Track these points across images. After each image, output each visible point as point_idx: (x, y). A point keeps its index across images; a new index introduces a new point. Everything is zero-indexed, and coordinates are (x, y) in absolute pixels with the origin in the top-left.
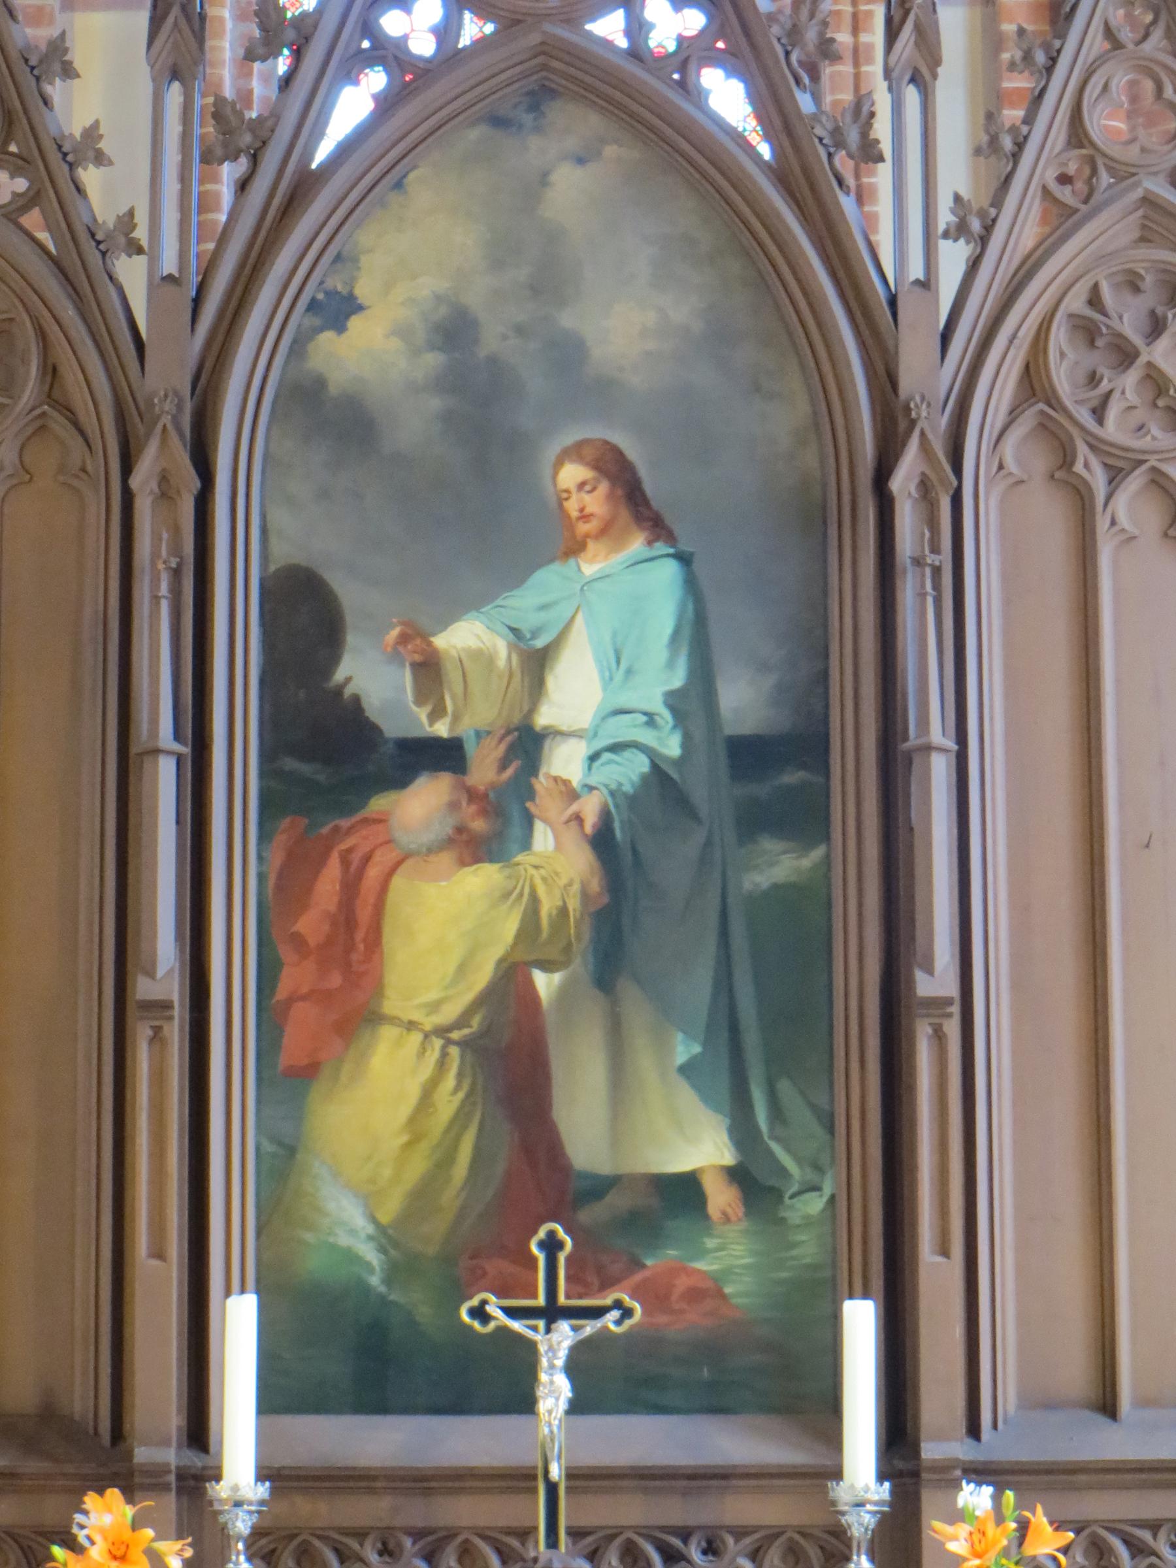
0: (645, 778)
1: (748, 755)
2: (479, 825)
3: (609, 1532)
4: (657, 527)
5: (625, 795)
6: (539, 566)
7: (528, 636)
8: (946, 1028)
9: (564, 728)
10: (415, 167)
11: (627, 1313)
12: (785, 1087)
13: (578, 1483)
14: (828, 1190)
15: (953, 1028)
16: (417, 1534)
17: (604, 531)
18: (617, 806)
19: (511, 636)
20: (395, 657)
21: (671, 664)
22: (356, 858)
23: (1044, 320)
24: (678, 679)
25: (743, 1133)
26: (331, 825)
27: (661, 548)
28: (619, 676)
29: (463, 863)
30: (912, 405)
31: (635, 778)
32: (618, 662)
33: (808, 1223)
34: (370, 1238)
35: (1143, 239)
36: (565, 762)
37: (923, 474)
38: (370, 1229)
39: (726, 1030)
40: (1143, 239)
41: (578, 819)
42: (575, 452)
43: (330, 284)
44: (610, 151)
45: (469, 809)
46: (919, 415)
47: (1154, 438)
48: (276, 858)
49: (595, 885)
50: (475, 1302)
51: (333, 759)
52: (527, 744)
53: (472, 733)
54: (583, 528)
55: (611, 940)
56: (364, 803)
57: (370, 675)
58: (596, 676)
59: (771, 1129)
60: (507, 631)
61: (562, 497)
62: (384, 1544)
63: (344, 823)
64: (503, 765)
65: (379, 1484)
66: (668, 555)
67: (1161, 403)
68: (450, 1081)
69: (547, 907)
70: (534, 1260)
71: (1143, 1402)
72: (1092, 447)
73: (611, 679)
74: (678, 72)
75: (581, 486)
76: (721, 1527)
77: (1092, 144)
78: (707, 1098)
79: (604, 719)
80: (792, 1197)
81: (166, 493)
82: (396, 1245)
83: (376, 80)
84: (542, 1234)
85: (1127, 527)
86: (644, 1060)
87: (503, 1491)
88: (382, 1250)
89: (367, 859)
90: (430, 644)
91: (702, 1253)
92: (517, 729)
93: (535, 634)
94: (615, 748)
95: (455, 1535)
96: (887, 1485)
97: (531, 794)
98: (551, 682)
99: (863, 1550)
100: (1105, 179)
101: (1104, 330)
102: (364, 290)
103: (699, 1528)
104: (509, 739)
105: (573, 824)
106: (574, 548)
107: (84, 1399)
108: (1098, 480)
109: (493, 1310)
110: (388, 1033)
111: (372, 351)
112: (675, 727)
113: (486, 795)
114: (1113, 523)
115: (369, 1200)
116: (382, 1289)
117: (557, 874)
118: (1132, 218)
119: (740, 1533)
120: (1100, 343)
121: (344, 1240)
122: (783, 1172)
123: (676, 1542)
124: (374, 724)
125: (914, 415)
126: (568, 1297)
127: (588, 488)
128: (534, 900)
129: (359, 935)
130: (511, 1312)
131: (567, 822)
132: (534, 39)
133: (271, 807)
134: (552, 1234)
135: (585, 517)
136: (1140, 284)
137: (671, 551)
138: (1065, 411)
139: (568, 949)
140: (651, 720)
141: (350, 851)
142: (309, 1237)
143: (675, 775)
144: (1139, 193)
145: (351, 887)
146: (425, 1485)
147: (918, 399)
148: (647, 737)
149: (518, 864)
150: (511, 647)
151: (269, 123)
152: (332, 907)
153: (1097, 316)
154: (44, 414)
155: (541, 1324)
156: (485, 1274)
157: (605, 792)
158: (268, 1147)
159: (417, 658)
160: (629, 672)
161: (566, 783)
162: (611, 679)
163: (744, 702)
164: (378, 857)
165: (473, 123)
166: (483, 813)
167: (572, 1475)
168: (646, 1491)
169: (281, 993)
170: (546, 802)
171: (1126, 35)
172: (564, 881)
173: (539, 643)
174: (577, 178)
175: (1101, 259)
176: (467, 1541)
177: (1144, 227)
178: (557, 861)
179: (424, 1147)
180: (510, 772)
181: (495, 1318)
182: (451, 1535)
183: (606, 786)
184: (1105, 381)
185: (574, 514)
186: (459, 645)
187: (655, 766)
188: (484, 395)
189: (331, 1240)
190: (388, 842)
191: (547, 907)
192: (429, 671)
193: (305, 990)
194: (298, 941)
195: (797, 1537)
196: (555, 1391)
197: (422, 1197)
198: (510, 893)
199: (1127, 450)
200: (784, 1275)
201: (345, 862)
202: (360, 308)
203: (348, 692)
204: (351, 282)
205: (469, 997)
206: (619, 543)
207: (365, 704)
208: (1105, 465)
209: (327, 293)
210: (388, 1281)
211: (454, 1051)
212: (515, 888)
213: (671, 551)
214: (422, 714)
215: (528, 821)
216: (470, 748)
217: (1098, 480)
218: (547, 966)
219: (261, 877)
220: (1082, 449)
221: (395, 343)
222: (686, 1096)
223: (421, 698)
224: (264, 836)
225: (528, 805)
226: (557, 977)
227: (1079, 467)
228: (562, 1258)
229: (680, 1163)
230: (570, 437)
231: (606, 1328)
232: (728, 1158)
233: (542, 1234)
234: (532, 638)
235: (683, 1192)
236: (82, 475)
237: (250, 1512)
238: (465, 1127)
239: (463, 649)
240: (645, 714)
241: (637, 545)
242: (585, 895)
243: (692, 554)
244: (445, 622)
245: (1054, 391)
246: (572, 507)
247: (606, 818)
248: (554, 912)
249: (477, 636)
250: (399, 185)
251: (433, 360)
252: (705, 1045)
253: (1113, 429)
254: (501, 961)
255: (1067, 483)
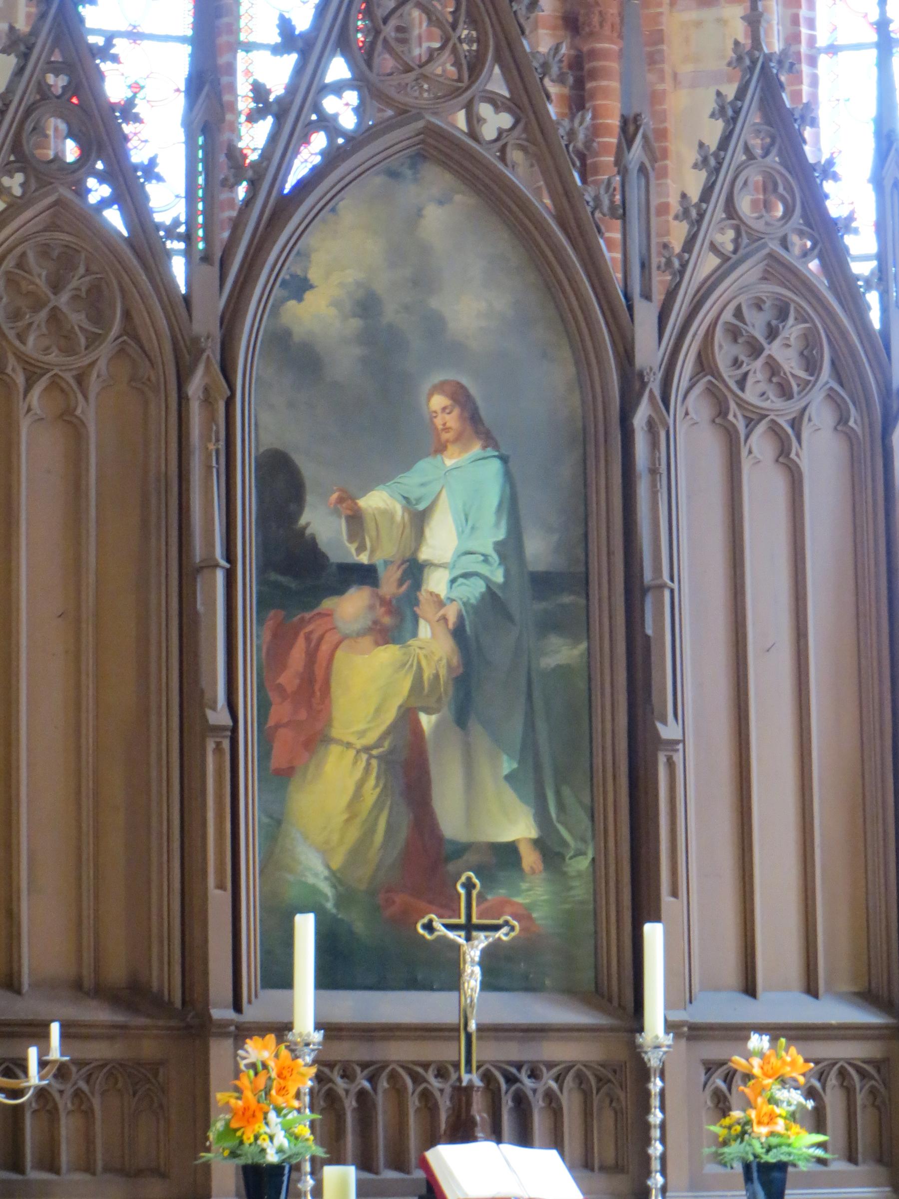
0: (483, 595)
1: (543, 583)
2: (387, 620)
3: (567, 1065)
4: (489, 440)
5: (473, 606)
6: (420, 459)
7: (414, 502)
8: (675, 758)
9: (436, 562)
10: (342, 199)
11: (513, 928)
12: (566, 791)
13: (333, 1033)
14: (590, 855)
15: (226, 744)
16: (364, 1065)
17: (457, 439)
18: (467, 612)
19: (404, 502)
20: (336, 512)
21: (497, 524)
22: (315, 636)
23: (709, 326)
24: (501, 535)
25: (542, 818)
26: (299, 616)
27: (490, 452)
28: (468, 530)
29: (377, 644)
30: (645, 374)
31: (477, 595)
32: (467, 521)
33: (580, 875)
34: (326, 878)
35: (764, 279)
36: (437, 583)
37: (650, 416)
38: (326, 873)
39: (529, 752)
40: (764, 279)
41: (444, 619)
42: (439, 388)
43: (293, 269)
44: (458, 198)
45: (381, 610)
46: (649, 379)
47: (772, 402)
48: (267, 636)
49: (455, 661)
50: (425, 920)
51: (301, 575)
52: (414, 571)
53: (382, 561)
54: (445, 436)
55: (465, 694)
56: (318, 603)
57: (321, 523)
58: (453, 529)
59: (558, 816)
60: (401, 498)
61: (433, 415)
62: (344, 1071)
63: (307, 615)
64: (401, 582)
65: (344, 1033)
66: (494, 456)
67: (775, 380)
68: (372, 781)
69: (427, 674)
70: (459, 895)
71: (35, 985)
72: (737, 404)
73: (463, 532)
74: (338, 136)
75: (444, 409)
76: (538, 1062)
77: (740, 219)
78: (522, 797)
79: (459, 556)
80: (571, 858)
81: (208, 400)
82: (340, 881)
83: (319, 141)
84: (463, 879)
85: (39, 412)
86: (484, 771)
87: (417, 1038)
88: (334, 886)
89: (321, 638)
90: (356, 504)
91: (519, 893)
92: (408, 561)
93: (419, 500)
94: (466, 576)
95: (388, 1066)
96: (671, 1035)
97: (416, 602)
98: (428, 533)
99: (658, 1075)
100: (745, 240)
101: (744, 332)
102: (314, 275)
103: (340, 1061)
104: (404, 566)
105: (442, 621)
106: (441, 449)
107: (166, 978)
108: (741, 425)
109: (437, 924)
110: (335, 749)
111: (318, 313)
112: (500, 564)
113: (390, 601)
114: (750, 452)
115: (325, 852)
116: (334, 911)
117: (432, 653)
118: (761, 265)
119: (550, 1065)
120: (740, 340)
121: (311, 880)
122: (564, 843)
123: (420, 1070)
124: (323, 553)
125: (646, 380)
126: (478, 918)
127: (448, 411)
128: (420, 668)
129: (317, 687)
130: (448, 927)
131: (438, 621)
132: (420, 124)
133: (264, 604)
134: (469, 879)
135: (446, 429)
136: (763, 306)
137: (496, 453)
138: (724, 381)
139: (439, 700)
140: (486, 559)
141: (311, 632)
142: (290, 877)
143: (500, 594)
144: (765, 252)
145: (311, 656)
146: (369, 1034)
147: (648, 370)
148: (484, 569)
149: (410, 646)
150: (405, 509)
151: (264, 164)
152: (301, 669)
153: (741, 324)
154: (124, 341)
155: (463, 934)
156: (394, 902)
157: (460, 603)
158: (266, 820)
159: (349, 513)
160: (473, 528)
161: (438, 596)
162: (463, 532)
163: (539, 549)
164: (327, 637)
165: (378, 174)
166: (389, 612)
167: (481, 1028)
168: (497, 1039)
169: (271, 723)
170: (426, 608)
171: (758, 152)
172: (436, 658)
173: (421, 507)
174: (441, 213)
175: (743, 289)
176: (393, 1070)
177: (766, 271)
178: (432, 645)
179: (358, 821)
180: (405, 587)
181: (438, 931)
182: (384, 1065)
183: (461, 599)
184: (745, 365)
185: (440, 427)
186: (374, 506)
187: (488, 588)
188: (388, 346)
189: (303, 879)
190: (334, 628)
191: (427, 674)
192: (356, 521)
193: (285, 720)
194: (280, 689)
195: (584, 1069)
196: (473, 977)
197: (357, 853)
198: (405, 664)
199: (757, 407)
200: (567, 906)
201: (308, 638)
202: (311, 287)
203: (308, 532)
204: (306, 270)
205: (383, 728)
206: (465, 448)
207: (318, 541)
208: (24, 369)
209: (291, 276)
210: (337, 905)
211: (374, 762)
212: (408, 661)
213: (496, 453)
214: (352, 548)
215: (416, 619)
216: (381, 569)
217: (741, 425)
218: (428, 711)
219: (259, 649)
220: (733, 406)
221: (333, 311)
222: (509, 795)
223: (352, 538)
224: (261, 621)
225: (416, 609)
226: (434, 718)
227: (731, 417)
228: (475, 893)
229: (507, 837)
230: (438, 377)
231: (499, 939)
232: (533, 834)
233: (463, 879)
234: (417, 504)
235: (507, 853)
236: (148, 383)
237: (313, 1050)
238: (381, 810)
239: (376, 508)
240: (483, 555)
241: (476, 449)
242: (449, 666)
243: (508, 457)
244: (366, 490)
245: (717, 367)
246: (439, 422)
247: (460, 618)
248: (432, 677)
249: (384, 501)
250: (333, 210)
251: (355, 324)
252: (519, 763)
253: (750, 395)
254: (400, 707)
255: (721, 425)
